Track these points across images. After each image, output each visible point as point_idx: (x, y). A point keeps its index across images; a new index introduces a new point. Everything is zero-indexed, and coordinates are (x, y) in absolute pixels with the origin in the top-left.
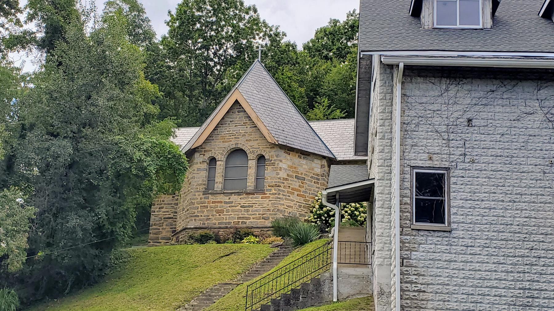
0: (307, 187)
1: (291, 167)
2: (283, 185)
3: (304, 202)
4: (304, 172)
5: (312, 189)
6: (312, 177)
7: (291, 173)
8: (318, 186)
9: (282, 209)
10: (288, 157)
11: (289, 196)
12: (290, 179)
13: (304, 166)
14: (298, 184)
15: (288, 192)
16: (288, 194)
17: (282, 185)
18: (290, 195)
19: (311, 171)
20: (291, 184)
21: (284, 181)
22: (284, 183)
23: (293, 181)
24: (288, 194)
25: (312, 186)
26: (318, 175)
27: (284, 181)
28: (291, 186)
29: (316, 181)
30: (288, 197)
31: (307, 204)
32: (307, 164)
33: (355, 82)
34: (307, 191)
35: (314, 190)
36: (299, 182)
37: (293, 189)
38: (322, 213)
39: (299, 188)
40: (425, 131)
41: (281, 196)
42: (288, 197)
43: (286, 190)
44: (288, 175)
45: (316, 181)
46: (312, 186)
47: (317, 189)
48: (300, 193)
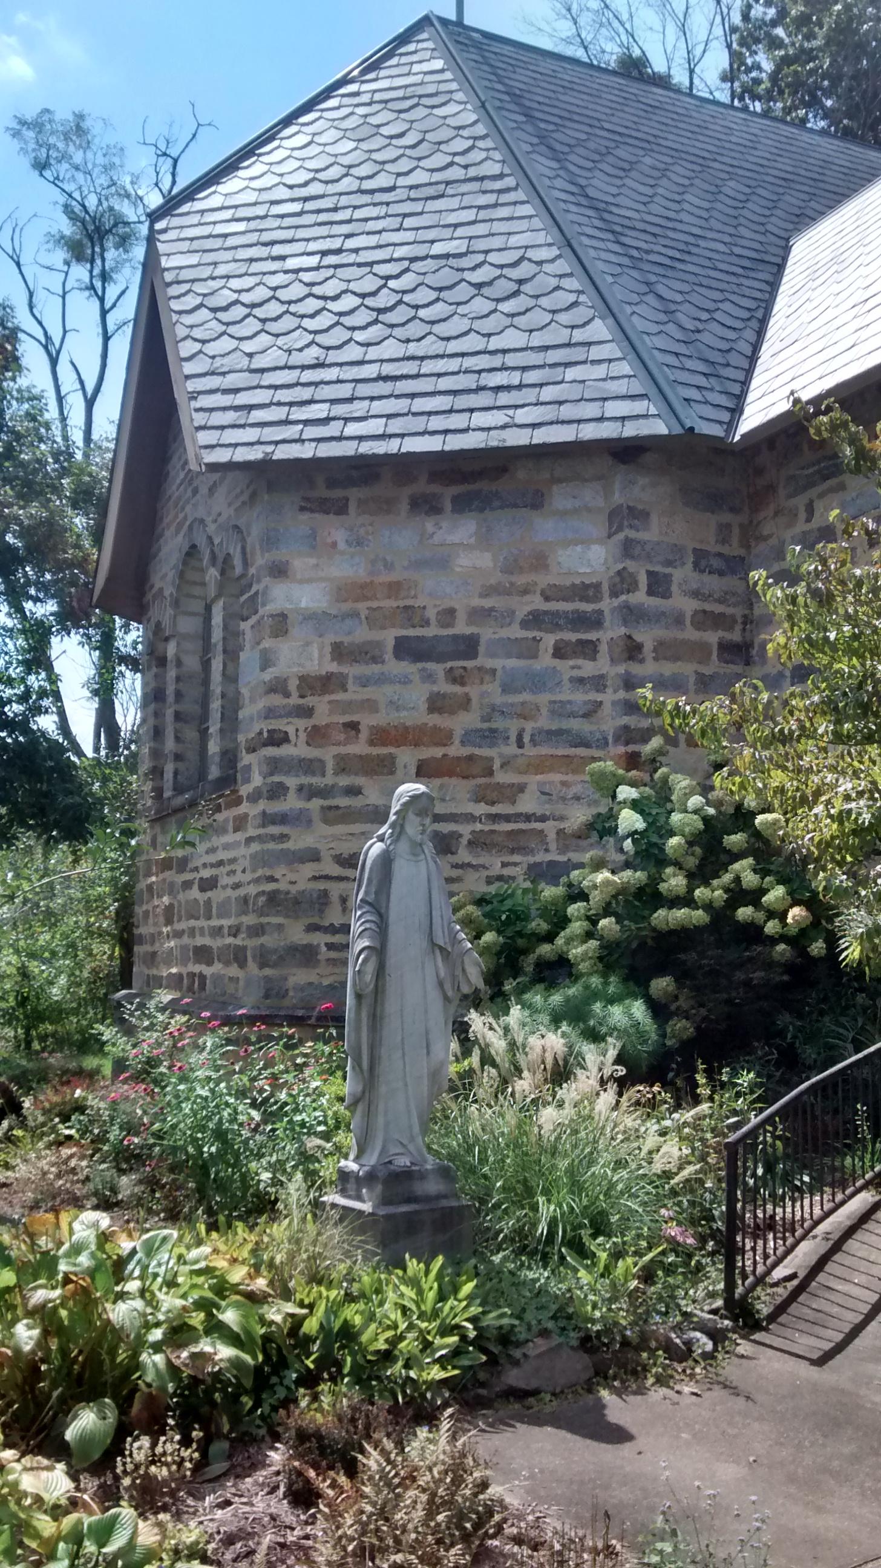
0: (499, 699)
1: (361, 591)
2: (302, 723)
3: (481, 809)
4: (464, 601)
5: (543, 699)
6: (535, 620)
7: (362, 634)
8: (588, 668)
9: (302, 886)
10: (336, 531)
11: (354, 791)
12: (352, 671)
13: (464, 561)
14: (417, 695)
15: (344, 765)
16: (344, 781)
17: (291, 726)
18: (359, 781)
19: (521, 580)
20: (371, 706)
21: (310, 701)
22: (307, 712)
23: (381, 680)
24: (344, 781)
25: (537, 682)
26: (587, 591)
27: (310, 701)
28: (367, 721)
29: (573, 637)
30: (343, 802)
31: (507, 818)
32: (484, 540)
33: (809, 1053)
34: (499, 723)
35: (559, 710)
36: (429, 677)
37: (380, 736)
38: (165, 1482)
39: (435, 720)
40: (313, 1021)
41: (292, 803)
42: (343, 802)
43: (328, 755)
44: (339, 652)
45: (573, 637)
46: (537, 682)
47: (580, 697)
48: (438, 752)
